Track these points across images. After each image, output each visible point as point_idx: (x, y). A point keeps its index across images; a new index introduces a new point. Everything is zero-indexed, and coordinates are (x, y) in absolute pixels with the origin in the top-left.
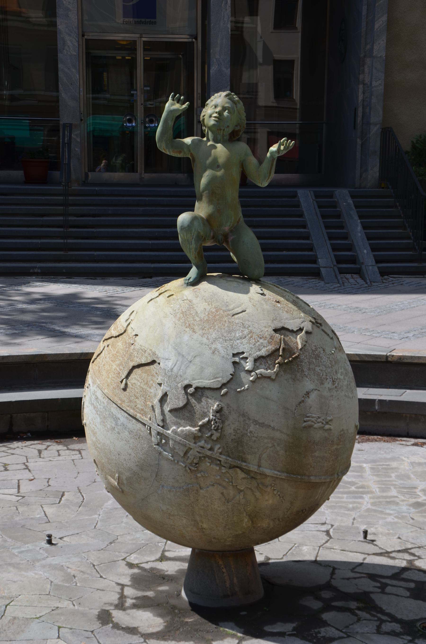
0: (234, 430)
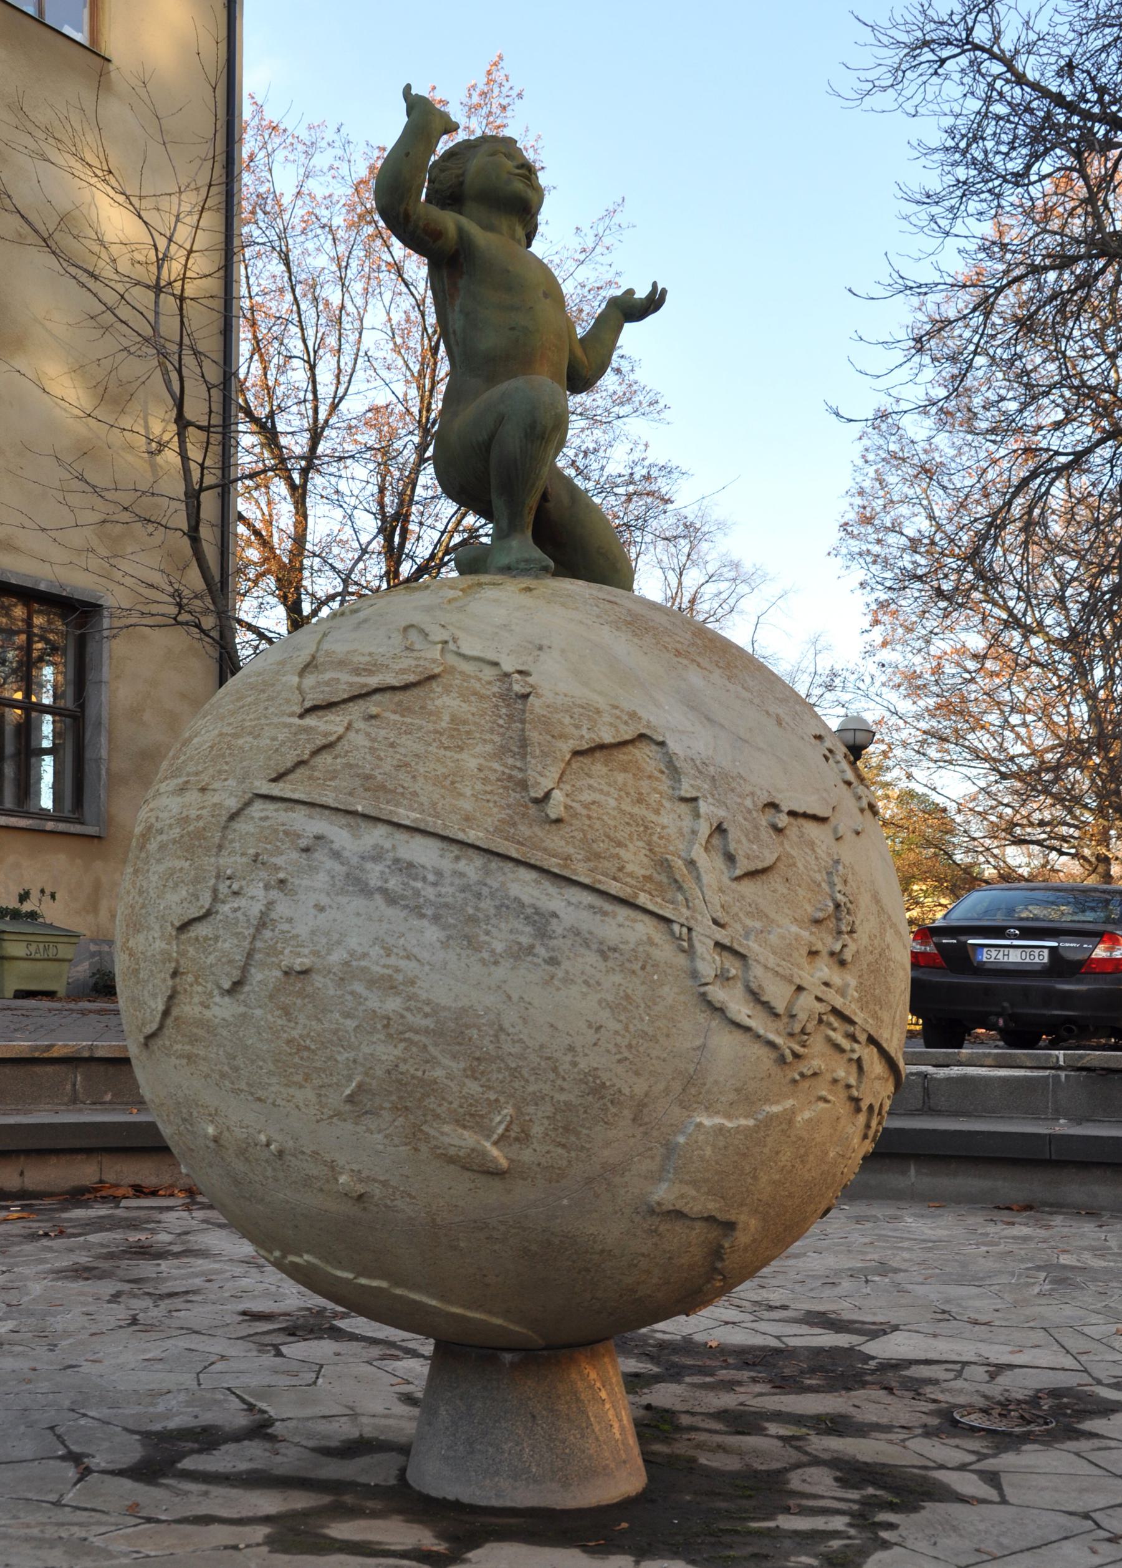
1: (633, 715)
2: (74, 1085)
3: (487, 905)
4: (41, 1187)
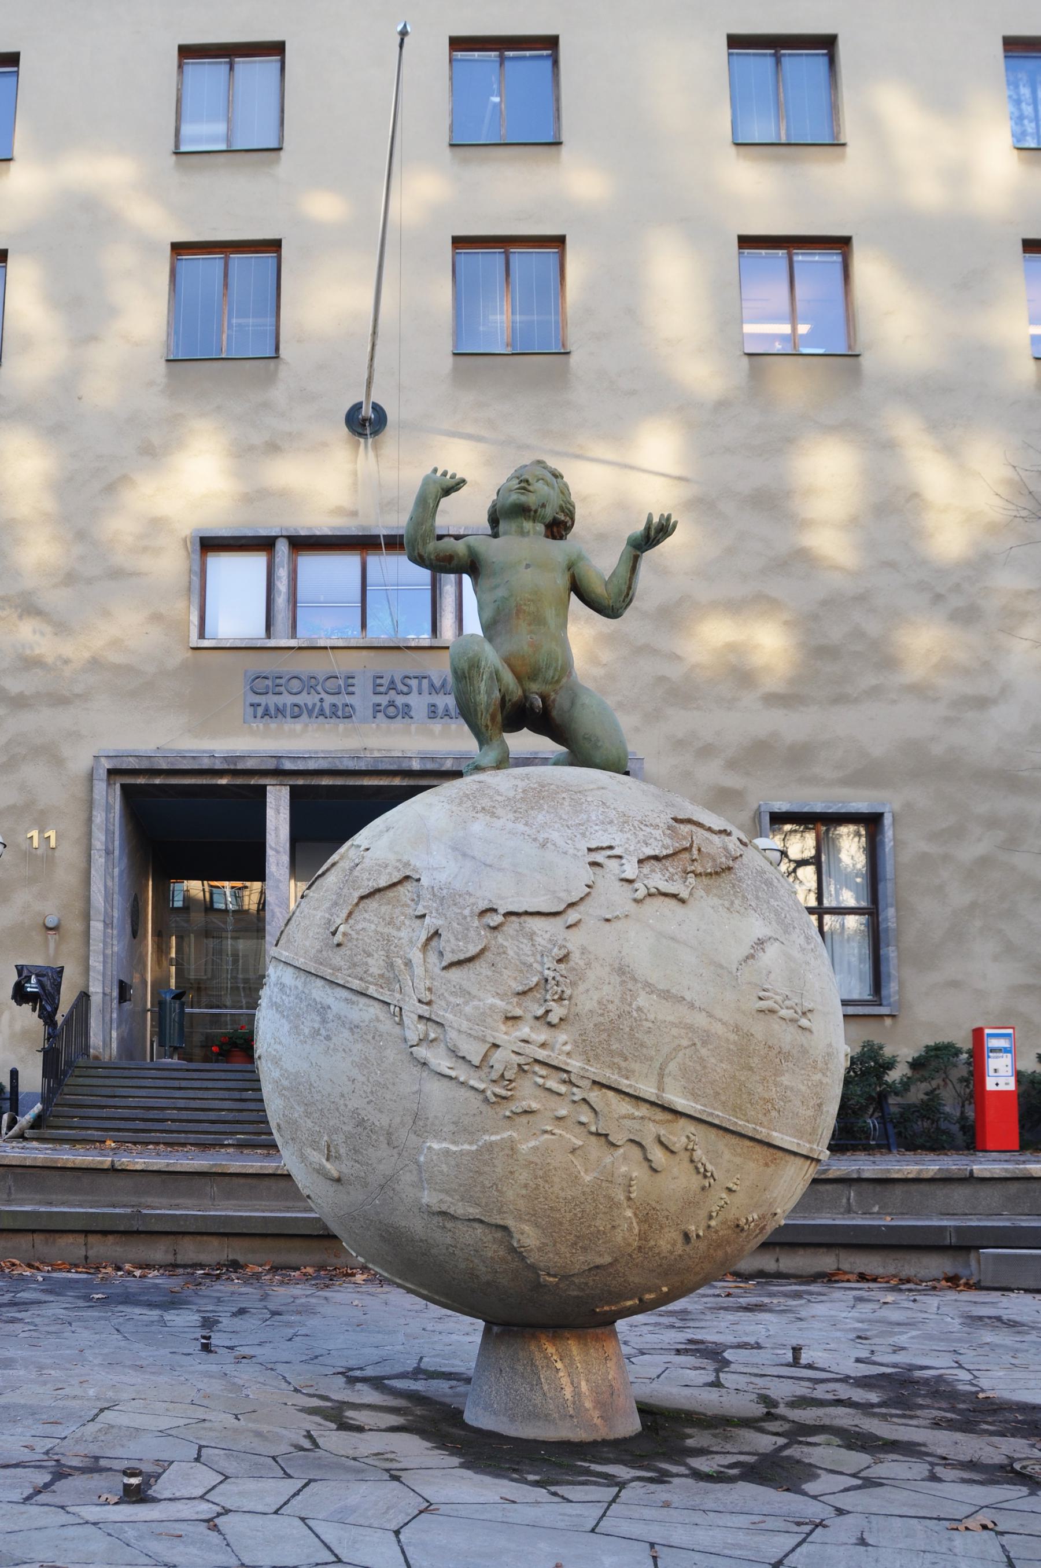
0: (599, 1003)
2: (849, 1199)
4: (792, 1271)
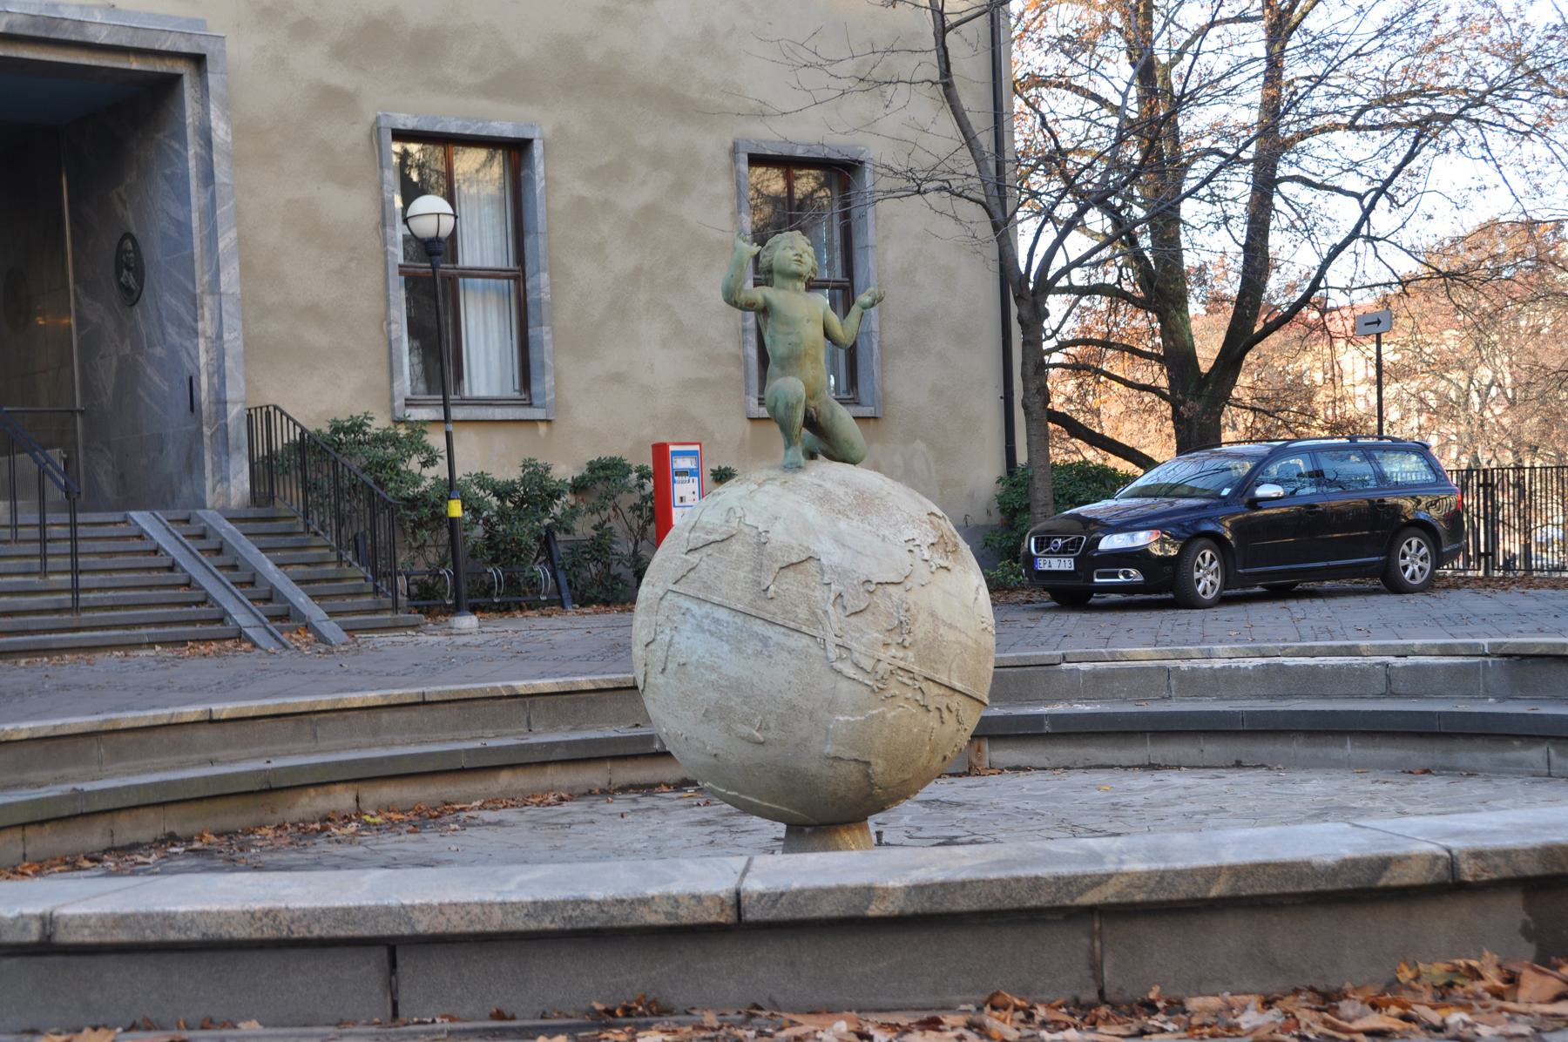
1: (808, 548)
3: (745, 635)
